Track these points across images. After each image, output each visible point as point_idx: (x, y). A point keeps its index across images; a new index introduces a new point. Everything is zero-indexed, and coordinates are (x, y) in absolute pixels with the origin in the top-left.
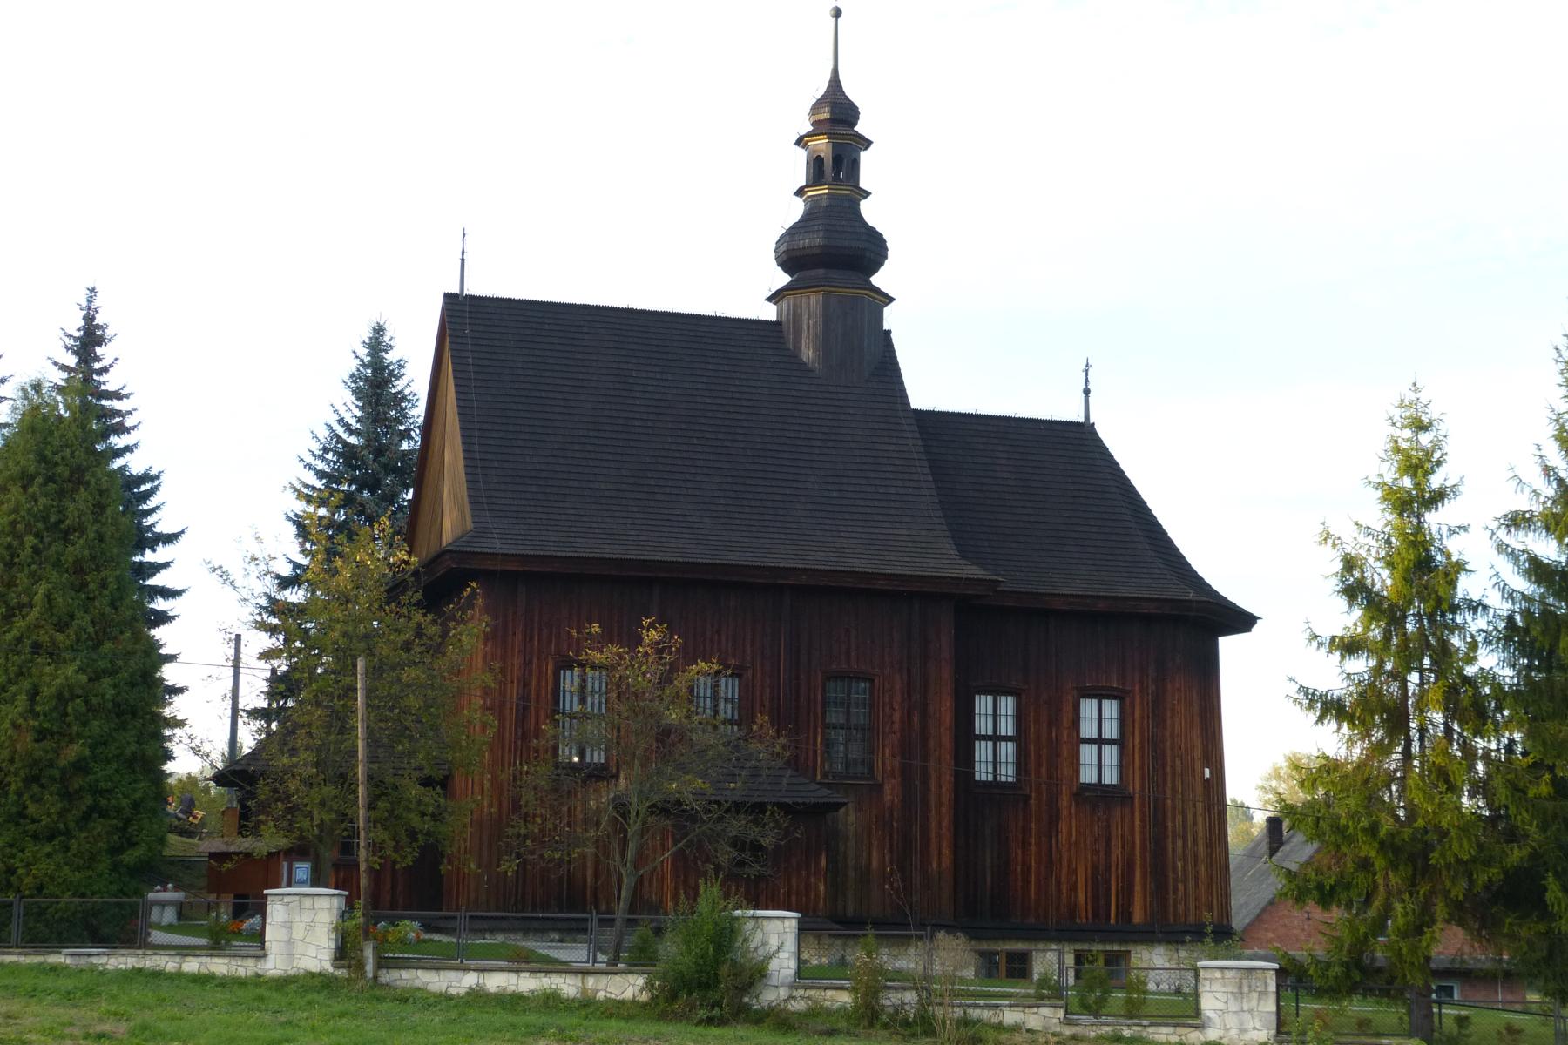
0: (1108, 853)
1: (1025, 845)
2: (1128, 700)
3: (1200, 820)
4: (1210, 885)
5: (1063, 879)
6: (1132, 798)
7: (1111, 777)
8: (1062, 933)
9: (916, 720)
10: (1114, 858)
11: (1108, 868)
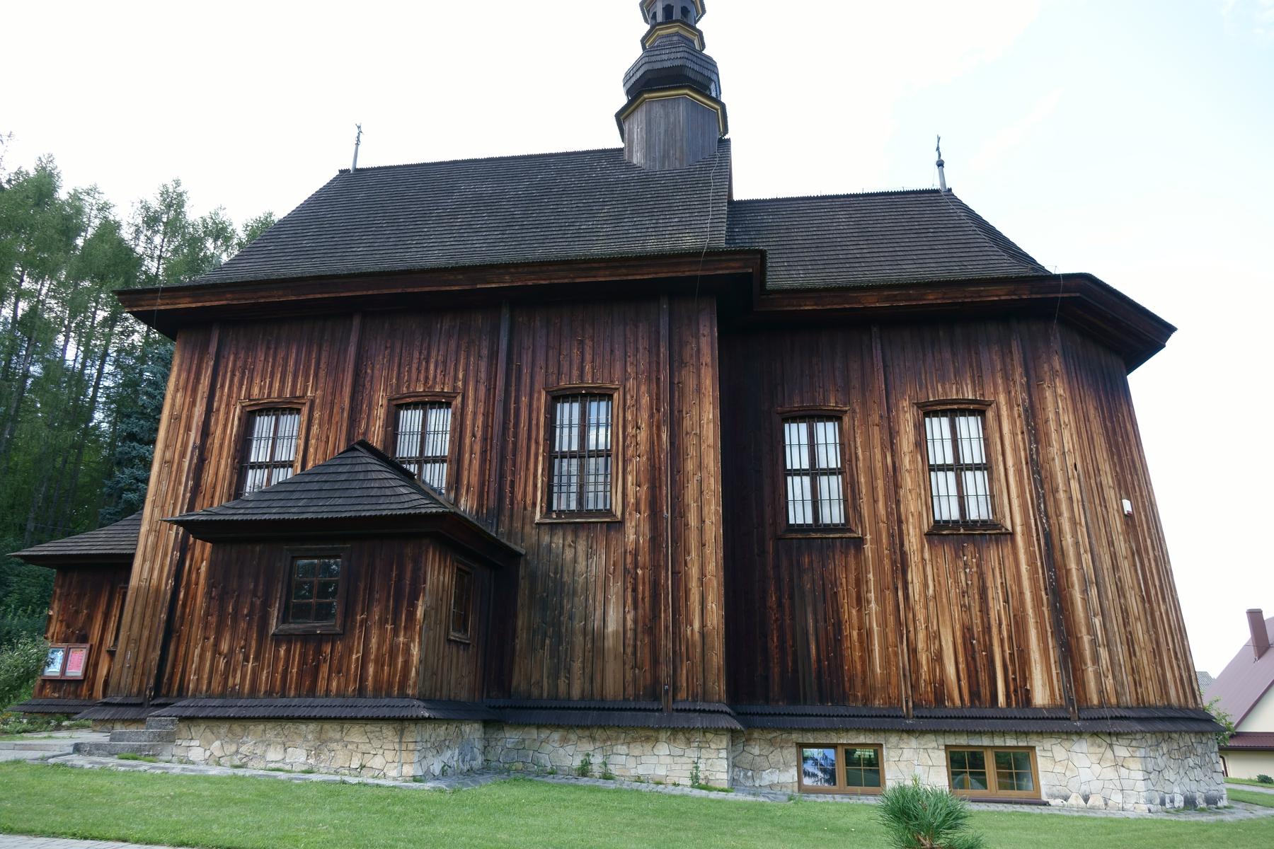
0: (985, 610)
1: (860, 601)
2: (990, 414)
3: (1125, 565)
4: (1157, 653)
6: (1012, 534)
7: (833, 514)
8: (924, 715)
9: (664, 437)
11: (987, 629)
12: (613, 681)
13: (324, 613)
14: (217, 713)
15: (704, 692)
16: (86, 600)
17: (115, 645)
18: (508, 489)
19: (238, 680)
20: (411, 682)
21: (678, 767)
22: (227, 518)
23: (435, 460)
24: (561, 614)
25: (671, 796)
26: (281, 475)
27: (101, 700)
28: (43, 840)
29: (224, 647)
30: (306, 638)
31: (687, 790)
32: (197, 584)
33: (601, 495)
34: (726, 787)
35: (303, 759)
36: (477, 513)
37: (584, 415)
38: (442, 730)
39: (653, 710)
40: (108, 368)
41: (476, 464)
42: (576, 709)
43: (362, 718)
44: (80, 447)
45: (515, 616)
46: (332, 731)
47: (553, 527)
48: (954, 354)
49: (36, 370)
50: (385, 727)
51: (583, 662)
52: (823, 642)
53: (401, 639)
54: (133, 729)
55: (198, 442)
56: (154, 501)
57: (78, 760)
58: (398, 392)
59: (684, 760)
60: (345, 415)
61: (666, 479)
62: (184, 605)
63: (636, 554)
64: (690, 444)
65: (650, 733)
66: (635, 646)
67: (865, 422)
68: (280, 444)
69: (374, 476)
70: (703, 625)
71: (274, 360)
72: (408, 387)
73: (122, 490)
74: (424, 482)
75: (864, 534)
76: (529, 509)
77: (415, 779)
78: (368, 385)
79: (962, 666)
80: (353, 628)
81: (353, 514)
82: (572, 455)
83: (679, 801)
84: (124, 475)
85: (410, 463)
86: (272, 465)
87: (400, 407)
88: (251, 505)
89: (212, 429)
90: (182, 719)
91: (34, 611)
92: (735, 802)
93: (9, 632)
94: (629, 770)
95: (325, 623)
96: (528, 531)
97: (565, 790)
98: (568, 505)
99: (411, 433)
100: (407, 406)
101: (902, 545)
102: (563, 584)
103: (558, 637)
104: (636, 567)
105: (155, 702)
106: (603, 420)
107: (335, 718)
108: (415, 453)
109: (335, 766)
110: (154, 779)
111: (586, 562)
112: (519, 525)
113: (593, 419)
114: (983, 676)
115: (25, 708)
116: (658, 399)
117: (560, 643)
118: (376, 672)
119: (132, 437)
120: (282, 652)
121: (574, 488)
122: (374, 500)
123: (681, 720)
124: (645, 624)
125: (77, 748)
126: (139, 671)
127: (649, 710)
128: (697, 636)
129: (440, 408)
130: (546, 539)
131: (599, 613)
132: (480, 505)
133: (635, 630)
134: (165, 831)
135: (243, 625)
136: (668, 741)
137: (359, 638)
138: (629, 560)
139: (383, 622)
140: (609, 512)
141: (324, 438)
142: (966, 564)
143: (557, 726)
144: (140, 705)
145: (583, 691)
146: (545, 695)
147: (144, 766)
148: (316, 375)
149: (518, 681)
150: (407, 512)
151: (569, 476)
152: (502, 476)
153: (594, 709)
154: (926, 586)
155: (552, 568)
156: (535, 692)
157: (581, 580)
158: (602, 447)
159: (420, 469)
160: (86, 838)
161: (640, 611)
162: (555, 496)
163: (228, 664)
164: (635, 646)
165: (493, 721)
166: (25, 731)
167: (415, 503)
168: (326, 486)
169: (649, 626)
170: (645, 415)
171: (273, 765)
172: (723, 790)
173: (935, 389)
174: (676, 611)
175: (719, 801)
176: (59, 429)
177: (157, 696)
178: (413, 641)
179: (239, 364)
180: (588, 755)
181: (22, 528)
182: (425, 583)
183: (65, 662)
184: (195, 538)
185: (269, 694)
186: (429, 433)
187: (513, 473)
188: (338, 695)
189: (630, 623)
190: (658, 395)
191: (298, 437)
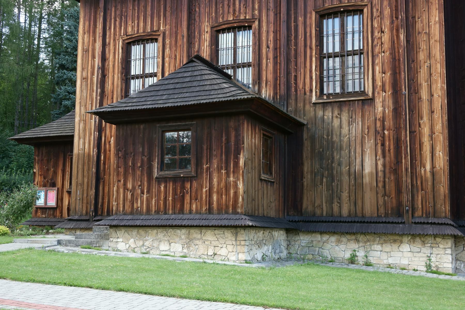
9: (402, 37)
12: (370, 204)
13: (184, 164)
14: (130, 223)
15: (435, 212)
16: (52, 163)
17: (70, 187)
18: (293, 82)
19: (139, 205)
20: (240, 205)
21: (416, 259)
22: (122, 109)
23: (244, 65)
24: (332, 162)
25: (411, 276)
26: (150, 81)
27: (67, 218)
28: (50, 286)
29: (130, 186)
30: (175, 179)
31: (423, 274)
32: (110, 151)
33: (357, 81)
34: (451, 272)
35: (180, 249)
36: (273, 98)
37: (343, 26)
38: (261, 234)
39: (398, 223)
40: (44, 26)
41: (271, 66)
42: (346, 222)
43: (212, 226)
44: (35, 76)
45: (302, 164)
46: (195, 233)
47: (324, 105)
49: (6, 30)
50: (226, 231)
51: (349, 193)
53: (232, 179)
54: (86, 233)
55: (100, 65)
56: (80, 103)
57: (60, 248)
58: (216, 22)
59: (420, 254)
60: (185, 40)
61: (404, 67)
62: (104, 164)
63: (383, 120)
64: (422, 41)
65: (396, 238)
66: (384, 182)
68: (148, 61)
69: (206, 77)
70: (433, 167)
71: (138, 8)
72: (223, 18)
73: (61, 100)
74: (238, 80)
76: (308, 94)
77: (246, 262)
78: (197, 19)
80: (202, 173)
81: (196, 102)
82: (335, 55)
83: (417, 279)
84: (61, 90)
85: (228, 69)
86: (144, 76)
87: (218, 32)
88: (135, 100)
89: (107, 56)
90: (111, 226)
91: (25, 172)
92: (457, 281)
93: (14, 184)
94: (383, 260)
95: (185, 170)
96: (307, 110)
97: (340, 271)
98: (335, 90)
99: (227, 49)
100: (223, 31)
102: (333, 143)
103: (332, 178)
104: (384, 129)
105: (96, 218)
106: (356, 28)
107: (197, 226)
108: (230, 62)
109: (199, 253)
110: (101, 258)
111: (347, 127)
112: (302, 105)
113: (350, 29)
115: (29, 223)
116: (397, 10)
117: (333, 180)
118: (218, 199)
119: (62, 67)
120: (162, 188)
121: (338, 78)
122: (208, 93)
123: (419, 229)
124: (391, 167)
125: (59, 242)
126: (85, 201)
127: (395, 223)
128: (429, 174)
129: (244, 30)
130: (320, 113)
131: (358, 160)
132: (275, 94)
133: (384, 172)
134: (111, 283)
135: (138, 173)
136: (409, 242)
137: (206, 178)
138: (378, 124)
139: (219, 169)
140: (363, 93)
141: (173, 57)
143: (334, 233)
144: (88, 220)
145: (350, 212)
146: (325, 213)
147: (95, 252)
148: (165, 15)
149: (306, 204)
150: (229, 99)
151: (334, 69)
152: (288, 73)
153: (358, 222)
155: (325, 132)
156: (318, 212)
157: (346, 139)
158: (356, 48)
159: (235, 72)
160: (71, 286)
161: (387, 159)
162: (325, 84)
163: (132, 195)
164: (384, 182)
165: (292, 229)
166: (32, 235)
167: (233, 93)
168: (178, 86)
169: (395, 169)
170: (387, 22)
171: (164, 253)
172: (448, 274)
174: (411, 111)
175: (446, 280)
176: (23, 65)
177: (96, 215)
178: (239, 180)
179: (118, 13)
180: (355, 251)
181: (12, 125)
182: (243, 143)
183: (46, 198)
184: (106, 122)
185: (157, 212)
186: (237, 47)
187: (296, 70)
188: (197, 213)
189: (380, 167)
190: (396, 7)
191: (158, 57)
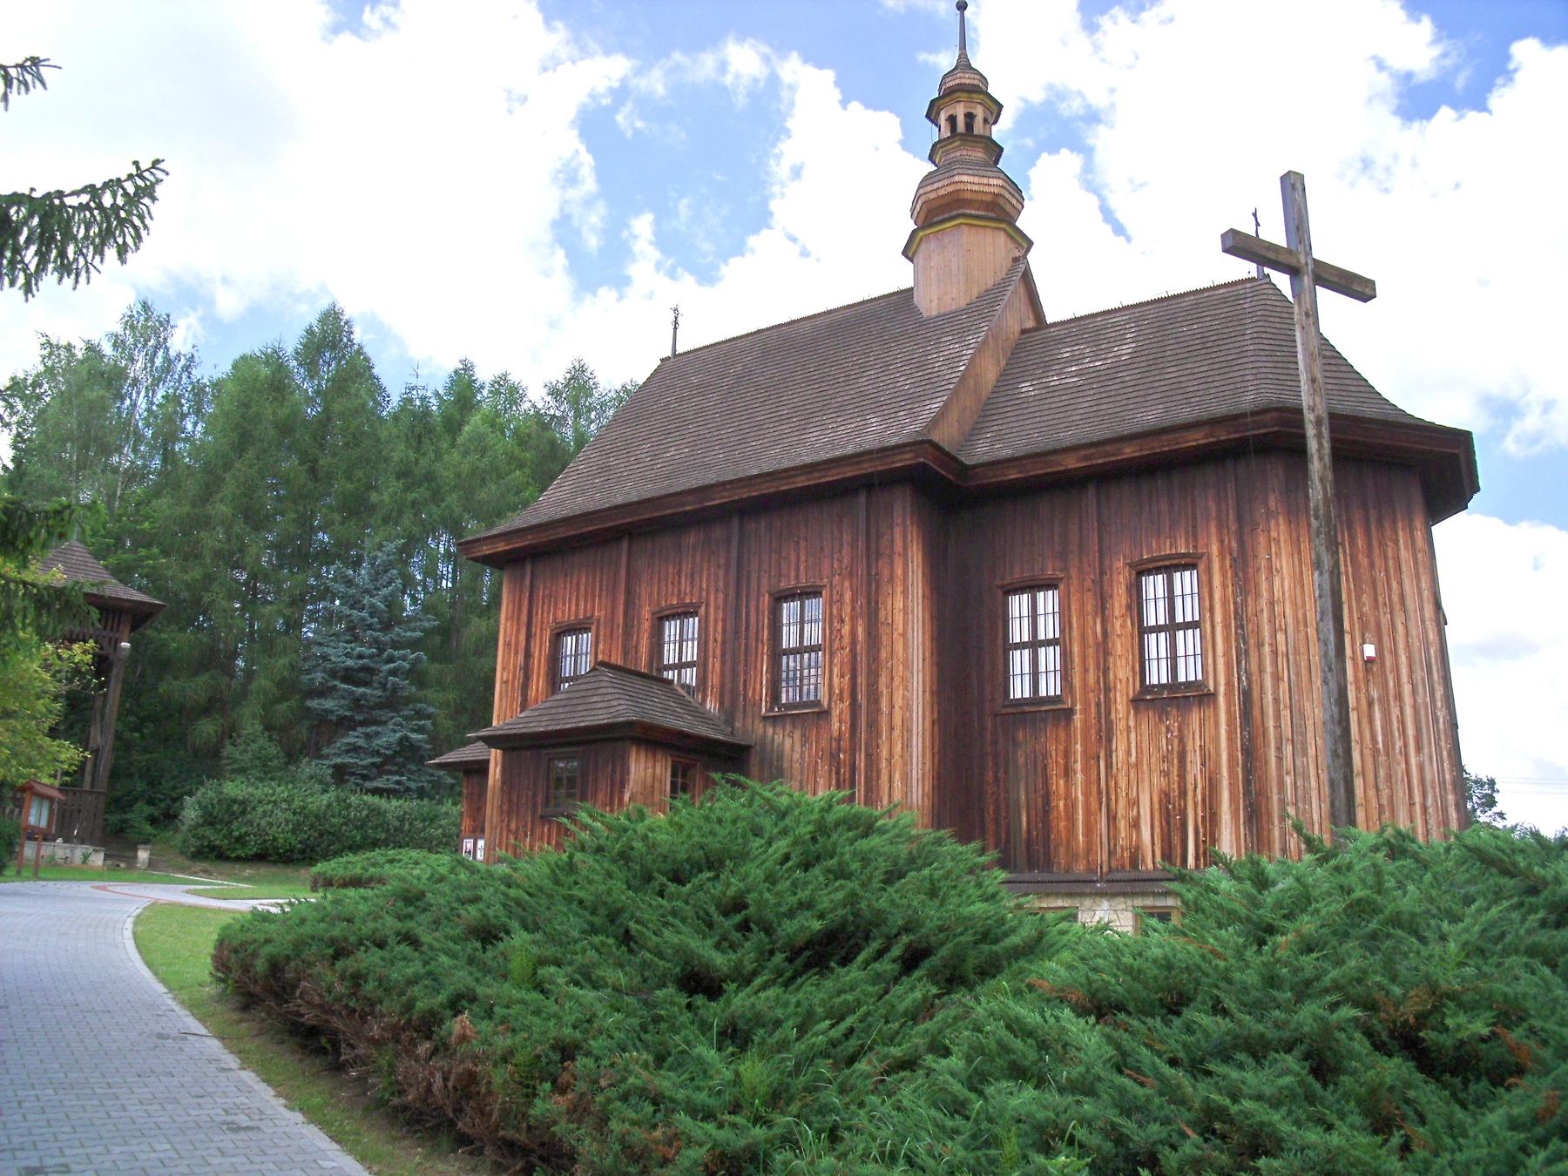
1: (1068, 772)
5: (1121, 812)
7: (1050, 686)
10: (1190, 779)
29: (513, 826)
41: (717, 665)
47: (774, 720)
48: (1171, 505)
52: (1033, 812)
63: (839, 740)
67: (1082, 590)
75: (1074, 704)
79: (1157, 830)
101: (1108, 713)
114: (1176, 840)
130: (770, 731)
132: (722, 704)
138: (834, 744)
140: (817, 703)
142: (1168, 728)
154: (1129, 753)
170: (847, 609)
173: (1149, 545)
